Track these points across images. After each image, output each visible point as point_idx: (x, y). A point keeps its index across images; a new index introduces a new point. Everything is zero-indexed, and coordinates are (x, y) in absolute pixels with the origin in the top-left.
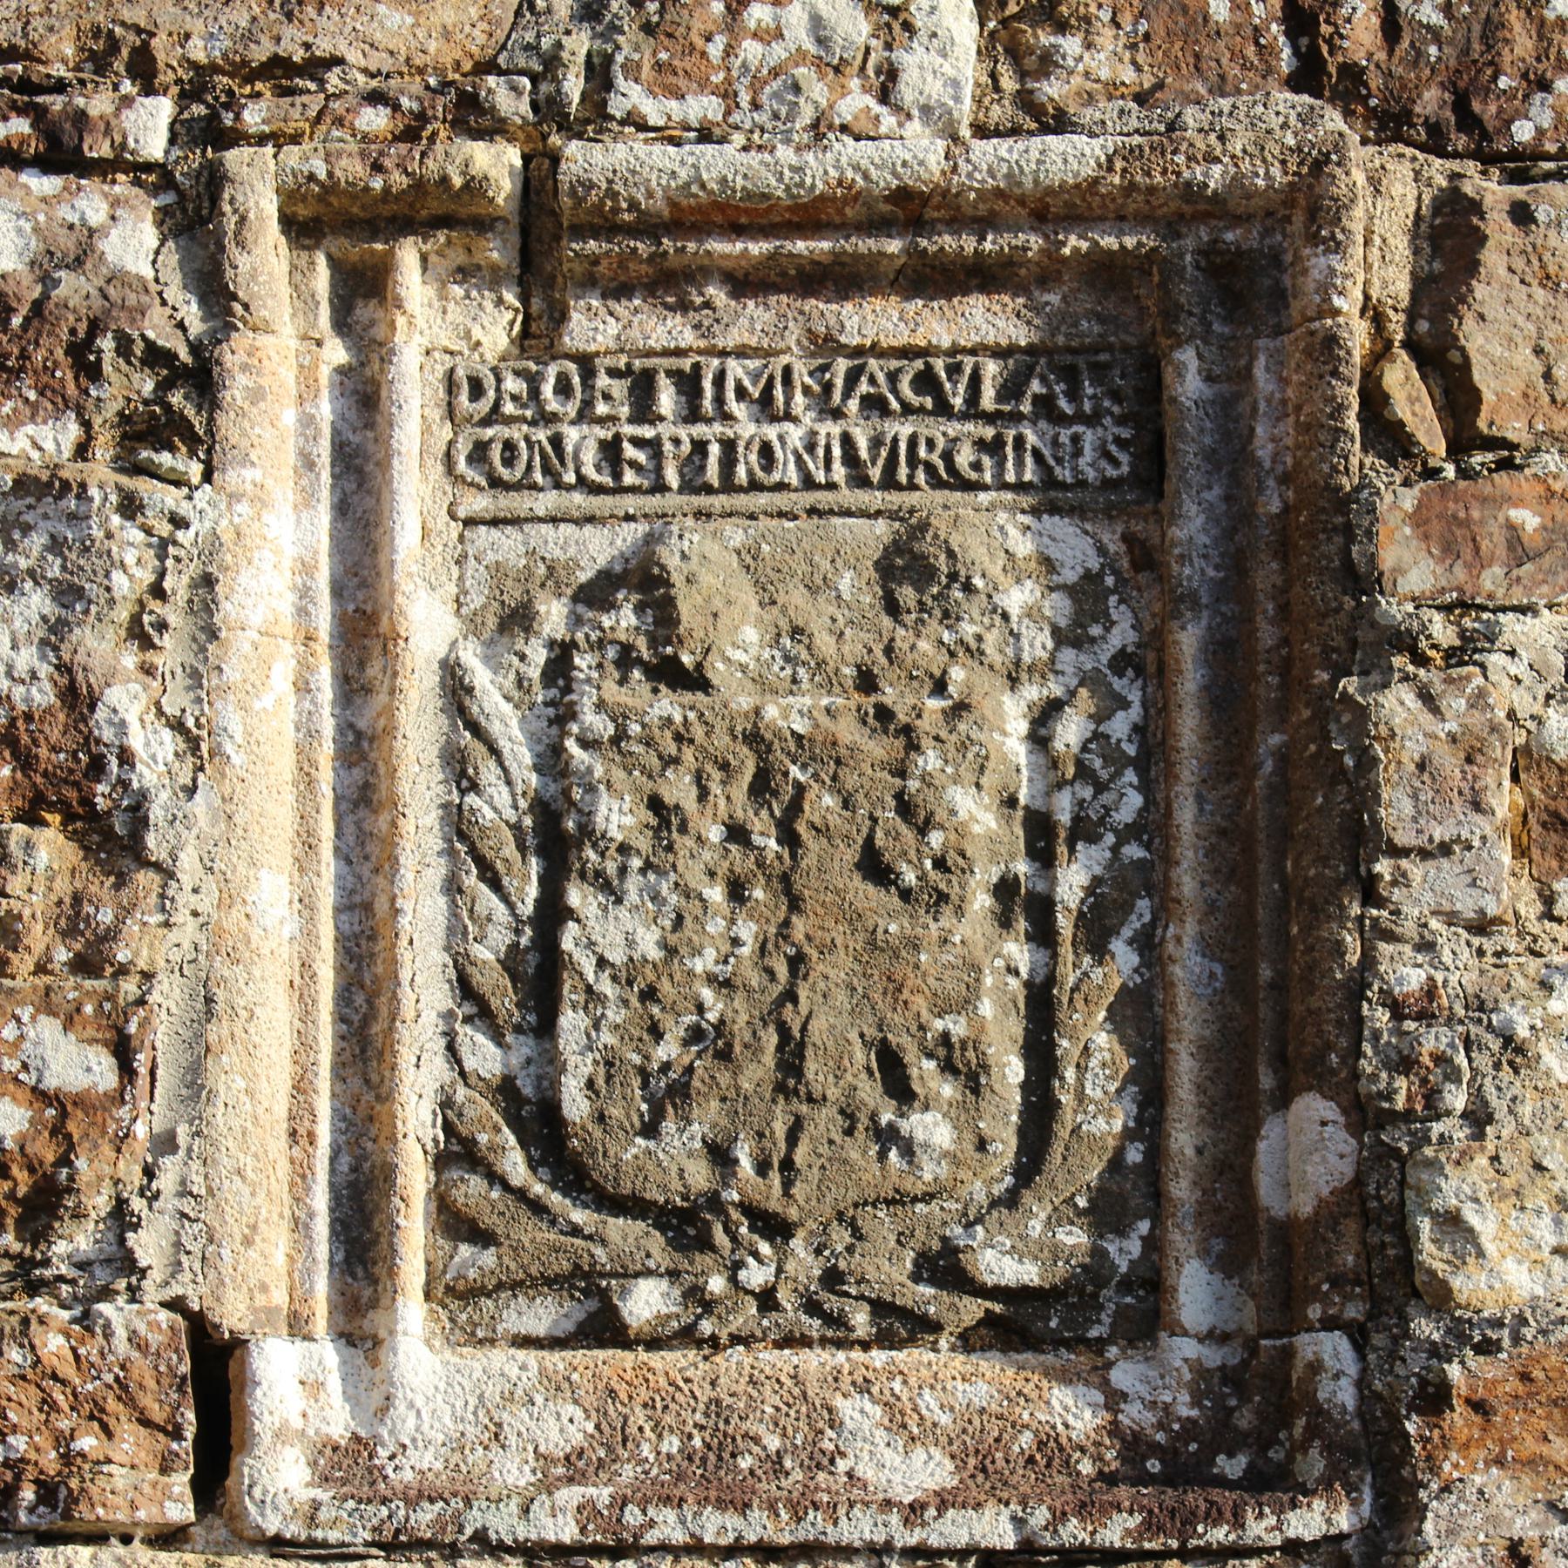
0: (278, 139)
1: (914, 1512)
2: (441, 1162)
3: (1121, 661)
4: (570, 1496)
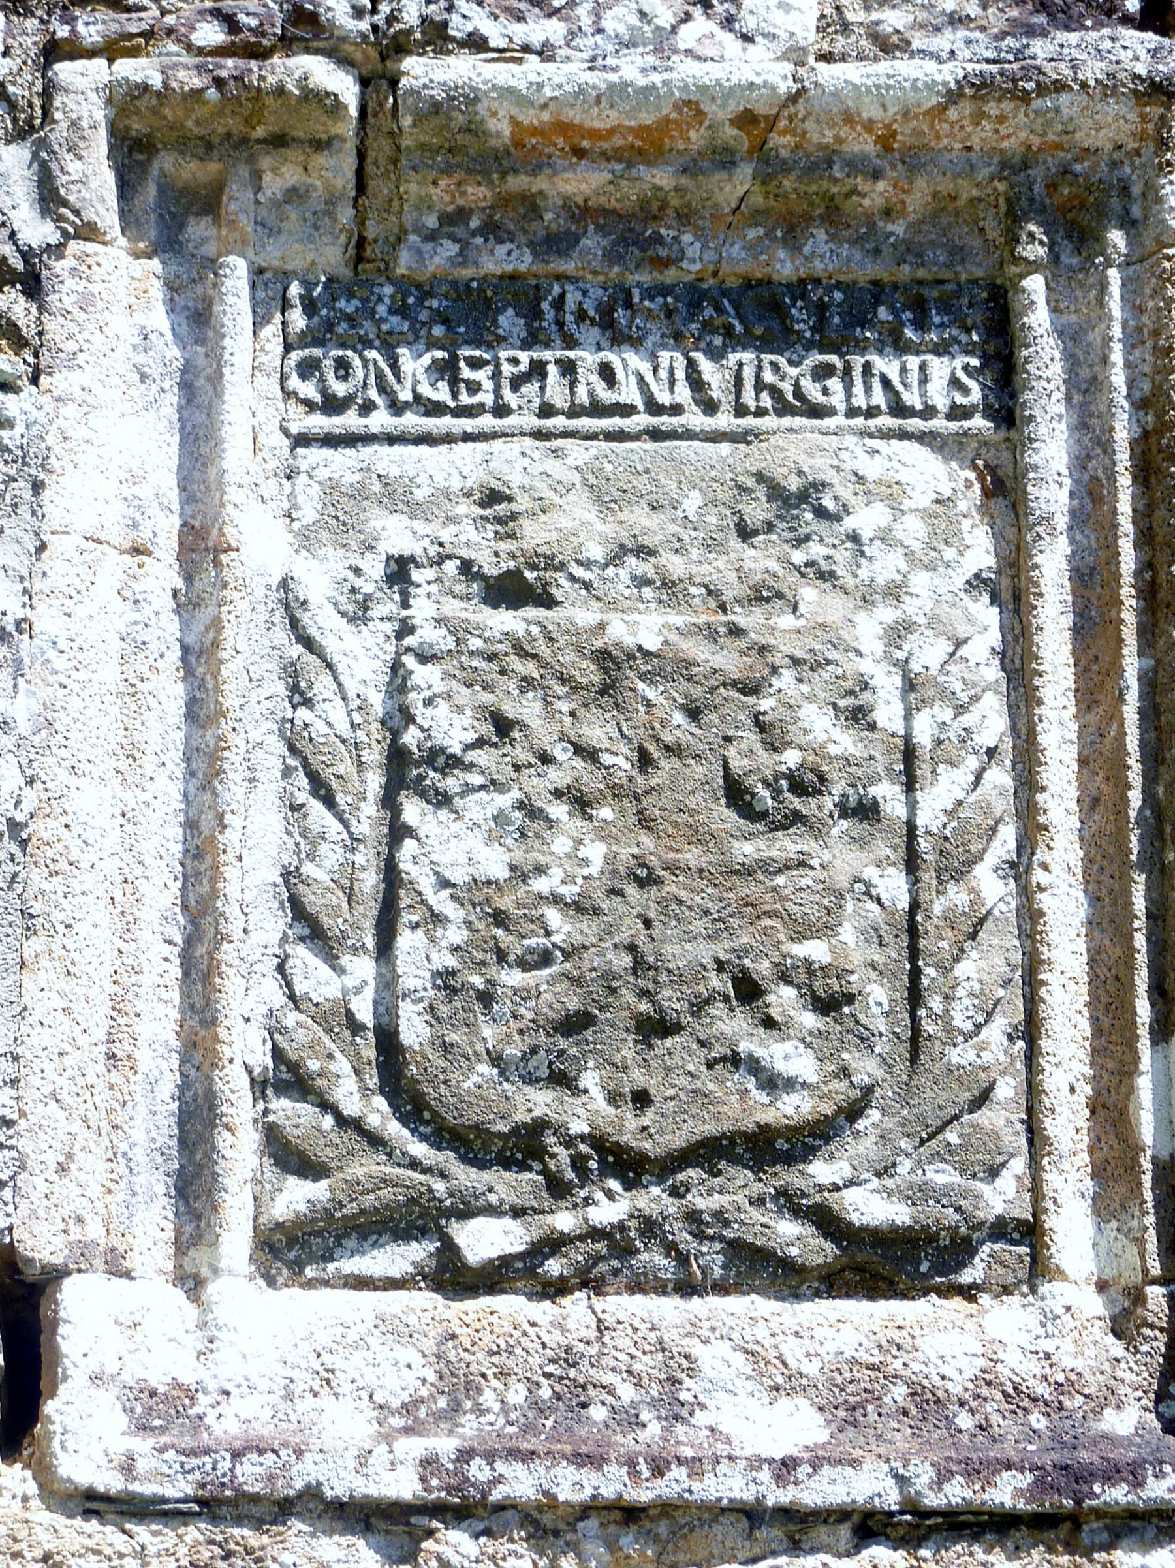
0: (112, 50)
1: (786, 1468)
2: (260, 1086)
3: (977, 583)
4: (413, 1448)
